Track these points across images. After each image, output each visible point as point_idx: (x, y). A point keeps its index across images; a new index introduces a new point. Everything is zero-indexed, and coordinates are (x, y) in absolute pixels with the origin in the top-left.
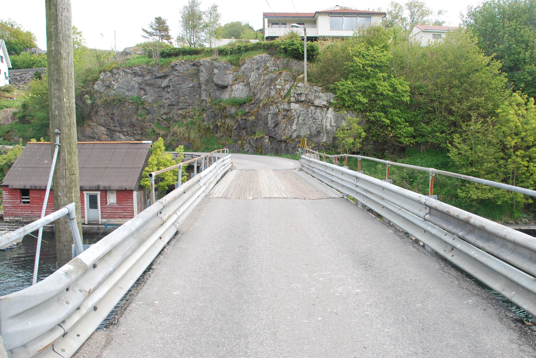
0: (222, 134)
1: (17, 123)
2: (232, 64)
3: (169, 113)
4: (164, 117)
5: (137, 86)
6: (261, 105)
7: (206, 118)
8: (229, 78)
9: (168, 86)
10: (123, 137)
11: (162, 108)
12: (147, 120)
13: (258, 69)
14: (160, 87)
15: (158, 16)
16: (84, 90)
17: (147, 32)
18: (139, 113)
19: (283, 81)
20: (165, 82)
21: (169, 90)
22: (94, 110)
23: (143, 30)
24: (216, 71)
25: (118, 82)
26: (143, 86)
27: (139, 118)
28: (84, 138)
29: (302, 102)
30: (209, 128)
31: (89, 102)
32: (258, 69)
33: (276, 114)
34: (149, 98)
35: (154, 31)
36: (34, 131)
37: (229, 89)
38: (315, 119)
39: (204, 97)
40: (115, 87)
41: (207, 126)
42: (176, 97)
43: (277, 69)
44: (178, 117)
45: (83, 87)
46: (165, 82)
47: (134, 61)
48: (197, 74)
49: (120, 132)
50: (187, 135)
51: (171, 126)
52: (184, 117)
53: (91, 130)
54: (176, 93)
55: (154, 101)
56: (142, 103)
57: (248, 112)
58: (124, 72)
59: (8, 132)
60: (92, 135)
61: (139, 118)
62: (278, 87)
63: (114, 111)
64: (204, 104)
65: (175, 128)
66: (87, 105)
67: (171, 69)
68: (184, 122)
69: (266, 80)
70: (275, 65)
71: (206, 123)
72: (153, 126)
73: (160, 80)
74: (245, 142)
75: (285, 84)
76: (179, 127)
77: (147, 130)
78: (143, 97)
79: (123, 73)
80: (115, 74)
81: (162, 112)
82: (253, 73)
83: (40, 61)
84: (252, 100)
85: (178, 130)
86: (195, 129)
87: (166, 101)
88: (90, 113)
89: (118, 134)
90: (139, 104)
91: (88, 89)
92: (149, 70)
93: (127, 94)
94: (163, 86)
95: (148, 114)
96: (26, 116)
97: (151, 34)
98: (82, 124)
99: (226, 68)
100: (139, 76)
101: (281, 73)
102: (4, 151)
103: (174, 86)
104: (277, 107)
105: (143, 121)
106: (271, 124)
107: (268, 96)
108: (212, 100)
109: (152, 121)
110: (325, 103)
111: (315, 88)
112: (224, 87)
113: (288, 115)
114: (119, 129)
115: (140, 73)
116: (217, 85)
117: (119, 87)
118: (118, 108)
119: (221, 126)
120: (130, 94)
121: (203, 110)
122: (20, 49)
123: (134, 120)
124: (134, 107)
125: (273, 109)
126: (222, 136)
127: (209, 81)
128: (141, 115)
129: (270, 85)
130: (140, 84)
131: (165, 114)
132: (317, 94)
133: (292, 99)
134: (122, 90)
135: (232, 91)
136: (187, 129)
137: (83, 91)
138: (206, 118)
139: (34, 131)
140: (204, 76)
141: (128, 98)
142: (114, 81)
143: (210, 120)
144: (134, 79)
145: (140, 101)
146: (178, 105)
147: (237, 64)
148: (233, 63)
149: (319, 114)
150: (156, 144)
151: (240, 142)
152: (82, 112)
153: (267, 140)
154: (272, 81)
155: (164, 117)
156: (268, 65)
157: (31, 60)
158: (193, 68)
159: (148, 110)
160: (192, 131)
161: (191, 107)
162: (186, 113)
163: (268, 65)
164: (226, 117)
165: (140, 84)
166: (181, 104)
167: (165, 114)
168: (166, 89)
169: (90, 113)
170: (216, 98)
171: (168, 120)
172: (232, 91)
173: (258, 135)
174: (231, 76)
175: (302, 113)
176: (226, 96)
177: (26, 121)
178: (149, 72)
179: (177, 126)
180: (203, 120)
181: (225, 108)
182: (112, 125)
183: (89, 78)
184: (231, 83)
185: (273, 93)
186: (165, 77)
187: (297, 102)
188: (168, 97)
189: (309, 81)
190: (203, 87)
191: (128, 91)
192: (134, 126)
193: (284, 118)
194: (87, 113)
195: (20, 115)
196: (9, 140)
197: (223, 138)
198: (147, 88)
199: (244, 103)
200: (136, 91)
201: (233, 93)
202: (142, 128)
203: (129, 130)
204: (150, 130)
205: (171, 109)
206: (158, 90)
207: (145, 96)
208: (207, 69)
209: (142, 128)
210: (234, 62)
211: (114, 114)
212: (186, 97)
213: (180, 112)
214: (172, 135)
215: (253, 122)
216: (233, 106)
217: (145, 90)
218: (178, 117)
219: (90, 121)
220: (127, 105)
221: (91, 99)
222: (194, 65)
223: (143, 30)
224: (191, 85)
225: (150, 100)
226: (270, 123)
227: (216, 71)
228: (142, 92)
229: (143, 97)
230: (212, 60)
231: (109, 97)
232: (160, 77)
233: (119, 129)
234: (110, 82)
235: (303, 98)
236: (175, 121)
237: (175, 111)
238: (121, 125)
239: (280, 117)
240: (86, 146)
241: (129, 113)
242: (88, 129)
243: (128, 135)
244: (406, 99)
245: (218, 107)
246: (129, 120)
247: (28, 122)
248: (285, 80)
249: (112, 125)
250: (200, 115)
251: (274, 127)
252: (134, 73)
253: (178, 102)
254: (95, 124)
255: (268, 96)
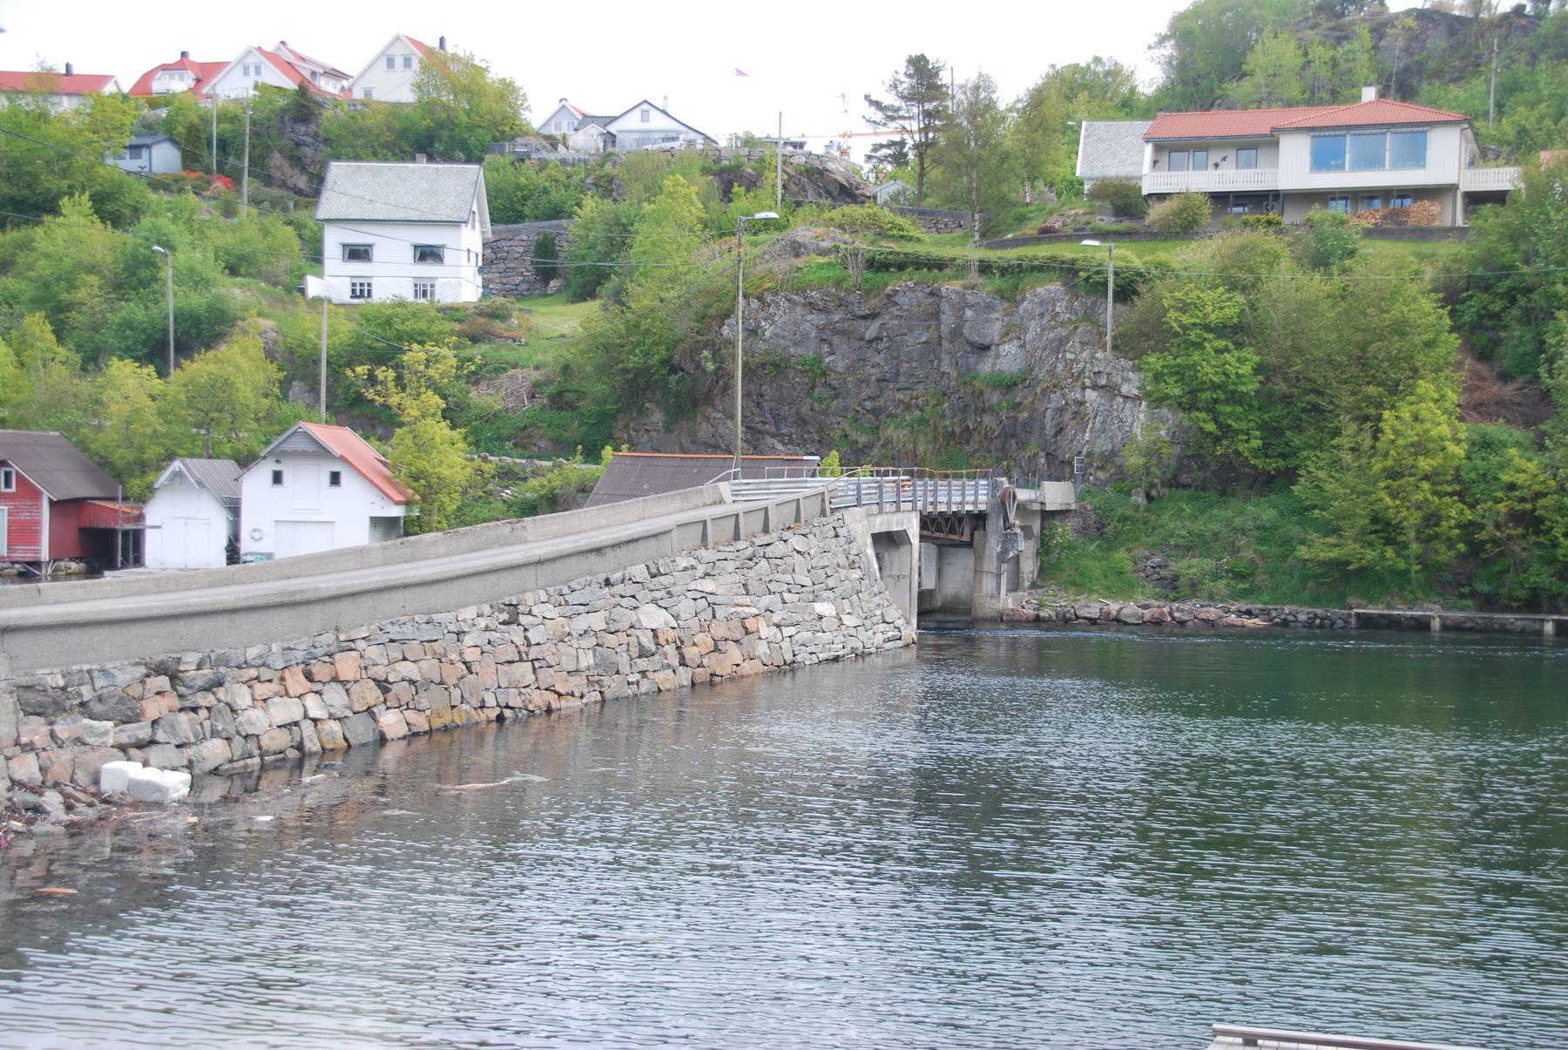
0: (976, 446)
1: (543, 408)
2: (1003, 298)
3: (878, 397)
4: (868, 404)
5: (813, 334)
6: (1038, 390)
7: (948, 413)
8: (995, 330)
9: (878, 339)
10: (780, 447)
11: (864, 385)
12: (832, 409)
13: (1042, 315)
14: (862, 339)
15: (915, 52)
16: (700, 338)
17: (877, 105)
18: (816, 395)
19: (1077, 345)
20: (872, 330)
21: (881, 346)
22: (721, 383)
23: (867, 98)
24: (969, 313)
25: (774, 322)
26: (827, 334)
27: (816, 405)
28: (694, 448)
29: (1103, 387)
30: (953, 432)
31: (710, 367)
32: (1042, 315)
33: (1061, 410)
34: (838, 362)
35: (903, 104)
36: (584, 429)
37: (992, 353)
38: (1121, 421)
39: (945, 368)
40: (767, 334)
41: (949, 429)
42: (894, 362)
43: (1073, 318)
44: (897, 407)
45: (698, 333)
46: (872, 330)
47: (811, 277)
48: (936, 315)
49: (774, 436)
50: (911, 446)
51: (882, 427)
52: (908, 407)
53: (711, 430)
54: (895, 354)
55: (848, 369)
56: (824, 374)
57: (1020, 404)
58: (789, 300)
59: (525, 428)
60: (713, 441)
61: (816, 405)
62: (1069, 356)
63: (764, 387)
64: (945, 381)
65: (890, 431)
66: (704, 370)
67: (885, 301)
68: (908, 418)
69: (1051, 342)
70: (1071, 309)
71: (947, 423)
72: (844, 425)
73: (863, 323)
74: (1012, 463)
75: (1082, 351)
76: (896, 428)
77: (832, 434)
78: (827, 360)
79: (787, 304)
80: (769, 305)
81: (863, 396)
82: (1033, 323)
83: (545, 188)
84: (1025, 380)
85: (895, 436)
86: (926, 435)
87: (873, 371)
88: (710, 390)
89: (769, 440)
90: (817, 373)
91: (709, 337)
92: (841, 299)
93: (792, 350)
94: (867, 337)
95: (836, 397)
96: (567, 391)
97: (891, 114)
98: (691, 415)
99: (990, 307)
100: (820, 310)
101: (1076, 328)
102: (533, 472)
103: (890, 339)
104: (1063, 396)
105: (825, 412)
106: (1050, 429)
107: (1052, 372)
108: (960, 375)
109: (842, 413)
110: (1136, 392)
111: (1123, 362)
112: (986, 348)
113: (1079, 411)
114: (773, 430)
115: (821, 304)
116: (971, 344)
117: (776, 335)
118: (772, 381)
119: (974, 429)
120: (800, 351)
121: (944, 394)
122: (482, 145)
123: (805, 410)
124: (806, 380)
125: (1056, 399)
126: (976, 451)
127: (956, 333)
128: (820, 400)
129: (1058, 352)
130: (821, 330)
131: (870, 398)
132: (1125, 374)
133: (1088, 382)
134: (782, 341)
135: (998, 356)
136: (912, 432)
137: (698, 342)
138: (948, 413)
139: (584, 429)
140: (948, 321)
141: (794, 360)
142: (765, 319)
143: (955, 416)
144: (809, 317)
145: (820, 368)
146: (897, 381)
147: (1010, 297)
148: (1006, 295)
149: (1128, 413)
150: (828, 460)
151: (1005, 463)
152: (693, 387)
153: (1043, 460)
154: (1061, 342)
155: (868, 404)
156: (1058, 309)
157: (518, 187)
158: (930, 300)
159: (835, 389)
160: (921, 438)
161: (921, 386)
162: (912, 399)
163: (1058, 309)
164: (984, 411)
165: (821, 330)
166: (902, 379)
167: (870, 398)
168: (874, 345)
169: (710, 390)
170: (969, 370)
171: (876, 412)
172: (998, 356)
173: (1032, 449)
174: (998, 325)
175: (1101, 409)
176: (986, 367)
177: (566, 403)
178: (841, 303)
179: (892, 426)
180: (943, 416)
181: (981, 393)
182: (758, 419)
183: (712, 311)
184: (996, 339)
185: (1060, 366)
186: (873, 316)
187: (1095, 387)
188: (877, 365)
189: (1115, 347)
190: (945, 343)
191: (795, 344)
192: (805, 423)
193: (1074, 418)
194: (705, 390)
195: (552, 389)
196: (524, 447)
197: (977, 455)
198: (836, 340)
199: (1015, 384)
200: (813, 345)
201: (998, 361)
202: (821, 429)
203: (793, 430)
204: (839, 433)
205: (882, 390)
206: (858, 344)
207: (831, 358)
208: (953, 307)
209: (821, 430)
210: (1007, 295)
211: (762, 396)
212: (914, 364)
213: (900, 396)
214: (884, 446)
215: (1025, 424)
216: (995, 389)
217: (830, 344)
218: (897, 407)
219: (710, 410)
220: (791, 376)
221: (714, 359)
222: (932, 294)
223: (867, 98)
224: (924, 339)
225: (840, 367)
226: (1048, 428)
227: (969, 313)
228: (826, 348)
229: (827, 360)
230: (966, 288)
231: (753, 356)
232: (863, 317)
233: (773, 430)
234: (757, 321)
235: (1103, 382)
236: (891, 416)
237: (892, 396)
238: (778, 419)
239: (1067, 416)
240: (711, 462)
241: (796, 394)
242: (704, 425)
243: (791, 442)
244: (1251, 387)
245: (969, 390)
246: (794, 410)
247: (572, 407)
248: (1081, 343)
249: (758, 419)
250: (938, 404)
251: (1055, 436)
252: (810, 303)
253: (898, 374)
254: (719, 415)
255: (1052, 372)
